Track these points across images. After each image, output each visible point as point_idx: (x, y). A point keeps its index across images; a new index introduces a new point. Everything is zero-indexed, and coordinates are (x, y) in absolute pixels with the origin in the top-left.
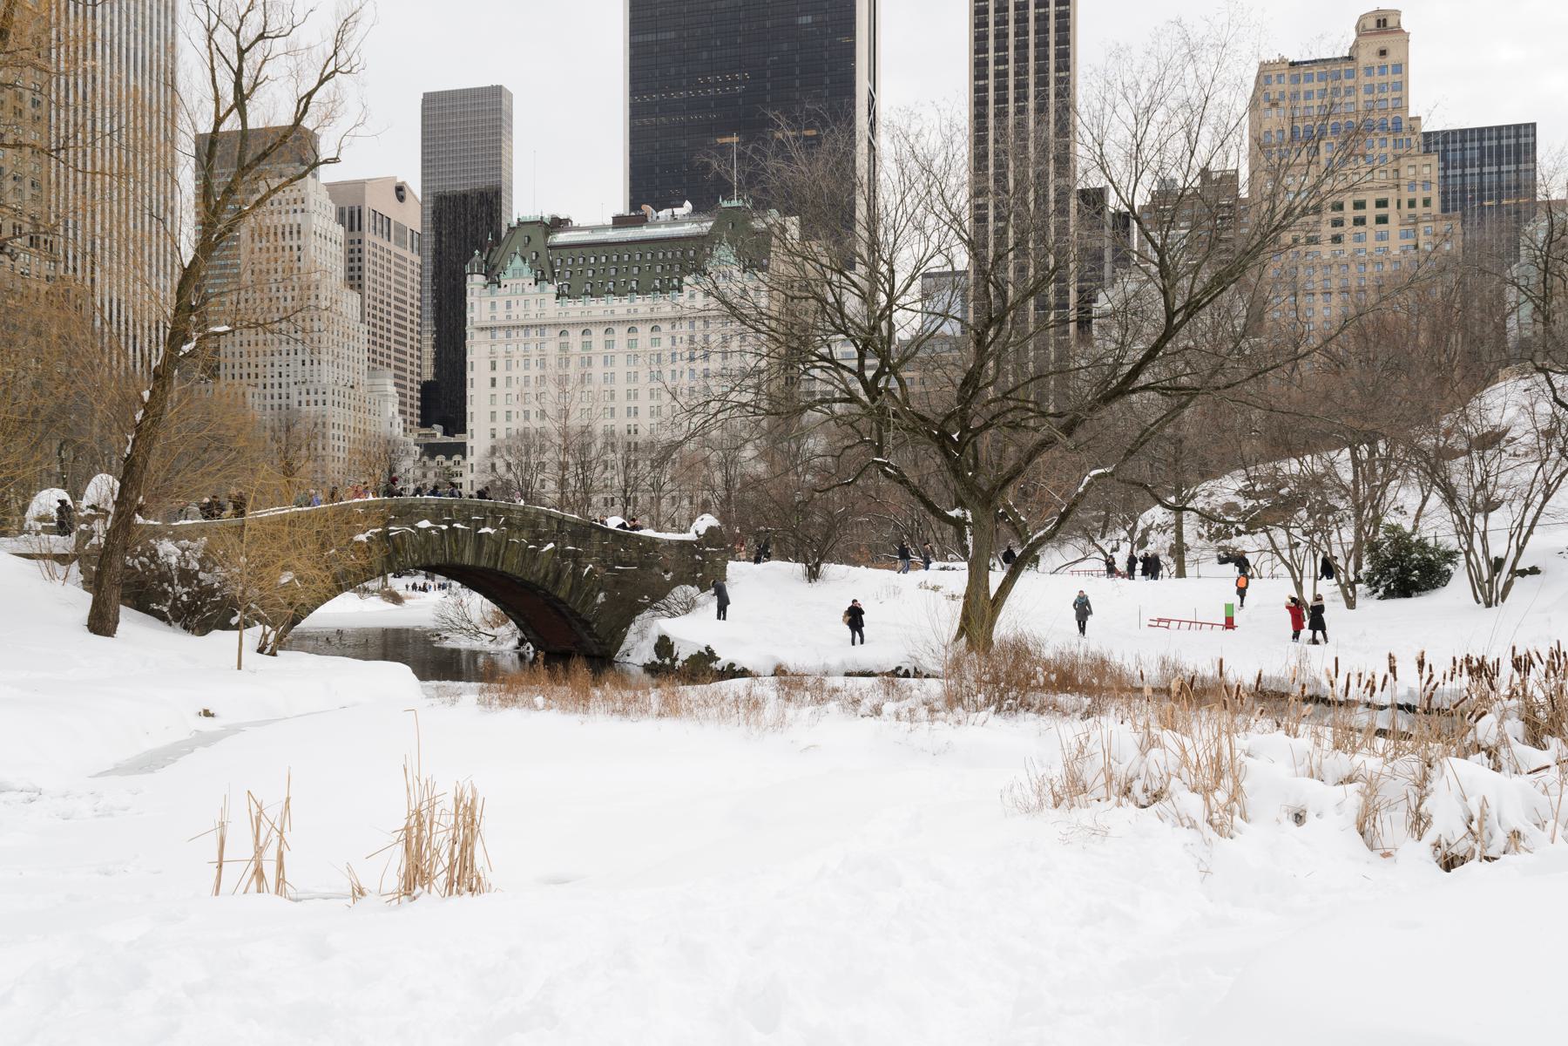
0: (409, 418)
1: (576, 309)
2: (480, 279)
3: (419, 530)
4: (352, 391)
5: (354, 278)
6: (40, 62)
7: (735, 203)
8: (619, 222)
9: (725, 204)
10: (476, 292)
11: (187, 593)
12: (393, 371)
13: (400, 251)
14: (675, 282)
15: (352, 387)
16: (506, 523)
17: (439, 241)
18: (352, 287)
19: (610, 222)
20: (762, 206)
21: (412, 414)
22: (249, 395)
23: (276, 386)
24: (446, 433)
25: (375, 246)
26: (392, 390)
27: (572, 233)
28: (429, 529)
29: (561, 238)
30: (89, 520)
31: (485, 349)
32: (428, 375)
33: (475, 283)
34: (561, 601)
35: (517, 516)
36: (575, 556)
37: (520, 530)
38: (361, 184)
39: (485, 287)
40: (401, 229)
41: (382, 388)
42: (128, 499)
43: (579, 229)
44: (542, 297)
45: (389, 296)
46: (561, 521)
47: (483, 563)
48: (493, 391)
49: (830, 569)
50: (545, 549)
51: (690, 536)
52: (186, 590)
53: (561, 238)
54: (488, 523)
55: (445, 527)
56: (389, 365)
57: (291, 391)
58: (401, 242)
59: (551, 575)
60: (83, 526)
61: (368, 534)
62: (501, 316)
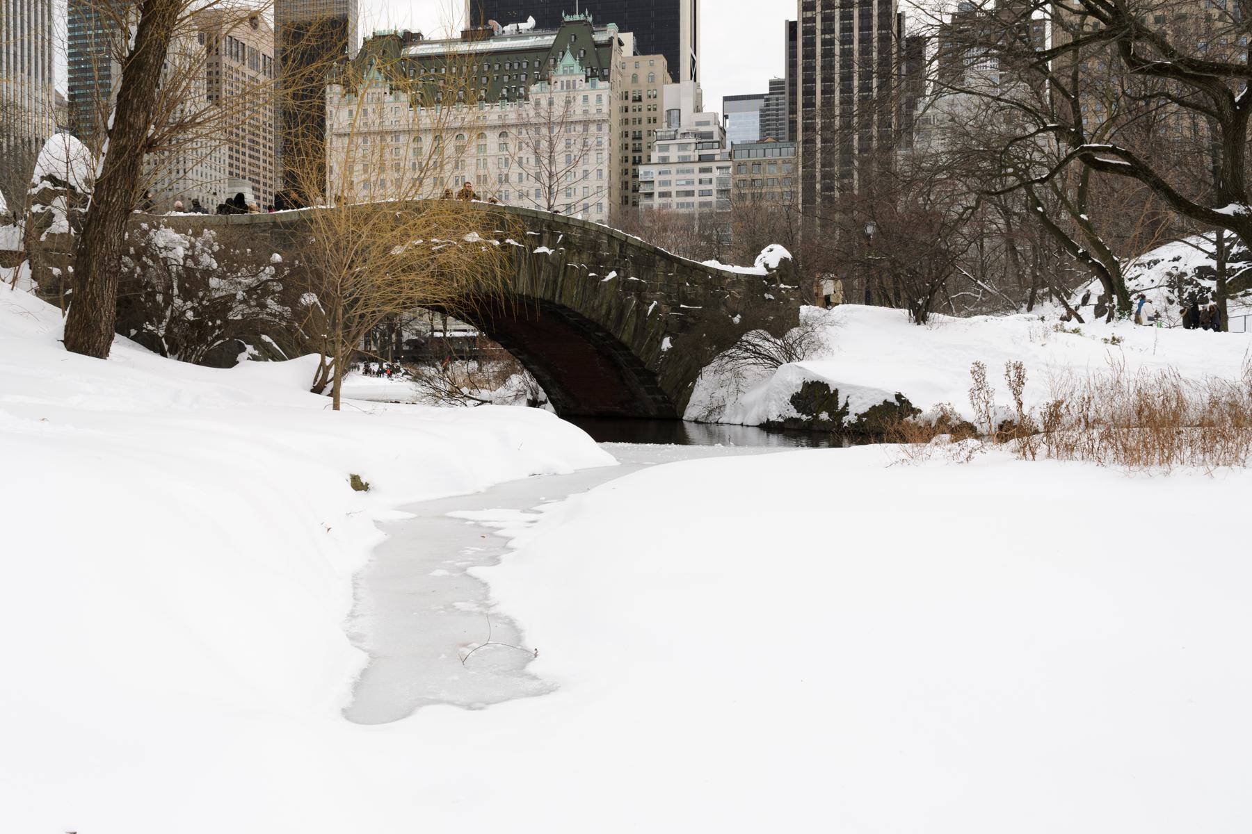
1: (427, 117)
2: (338, 88)
3: (467, 244)
4: (215, 198)
7: (577, 17)
9: (568, 18)
10: (336, 100)
11: (193, 308)
13: (253, 73)
14: (522, 90)
15: (215, 194)
16: (566, 242)
19: (459, 36)
20: (601, 22)
25: (231, 68)
27: (424, 46)
28: (478, 244)
29: (414, 50)
30: (45, 198)
33: (334, 92)
34: (624, 347)
35: (576, 234)
36: (638, 289)
37: (580, 253)
40: (254, 53)
42: (131, 126)
46: (624, 243)
47: (539, 293)
50: (607, 278)
51: (758, 269)
52: (189, 304)
53: (414, 50)
54: (545, 241)
58: (254, 66)
59: (613, 312)
60: (36, 208)
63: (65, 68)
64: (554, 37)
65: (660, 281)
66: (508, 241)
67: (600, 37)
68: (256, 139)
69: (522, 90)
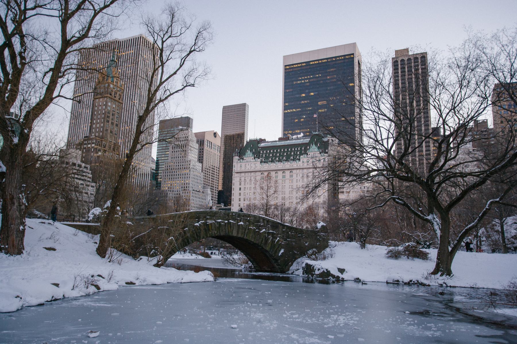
0: (214, 202)
2: (237, 158)
5: (201, 159)
6: (120, 101)
7: (317, 133)
8: (280, 139)
12: (210, 187)
14: (298, 157)
17: (225, 148)
18: (200, 162)
19: (277, 140)
21: (215, 200)
22: (168, 194)
23: (171, 175)
24: (225, 206)
26: (209, 192)
27: (266, 143)
29: (262, 145)
31: (238, 179)
32: (220, 188)
33: (236, 158)
34: (267, 251)
38: (203, 133)
39: (239, 160)
41: (207, 192)
43: (268, 142)
44: (256, 162)
45: (209, 178)
47: (240, 235)
48: (240, 192)
49: (368, 246)
54: (242, 220)
55: (226, 222)
56: (209, 185)
57: (180, 192)
59: (264, 241)
61: (200, 223)
62: (243, 169)
63: (156, 151)
64: (309, 139)
65: (280, 232)
66: (230, 221)
67: (325, 139)
68: (214, 170)
69: (298, 157)
